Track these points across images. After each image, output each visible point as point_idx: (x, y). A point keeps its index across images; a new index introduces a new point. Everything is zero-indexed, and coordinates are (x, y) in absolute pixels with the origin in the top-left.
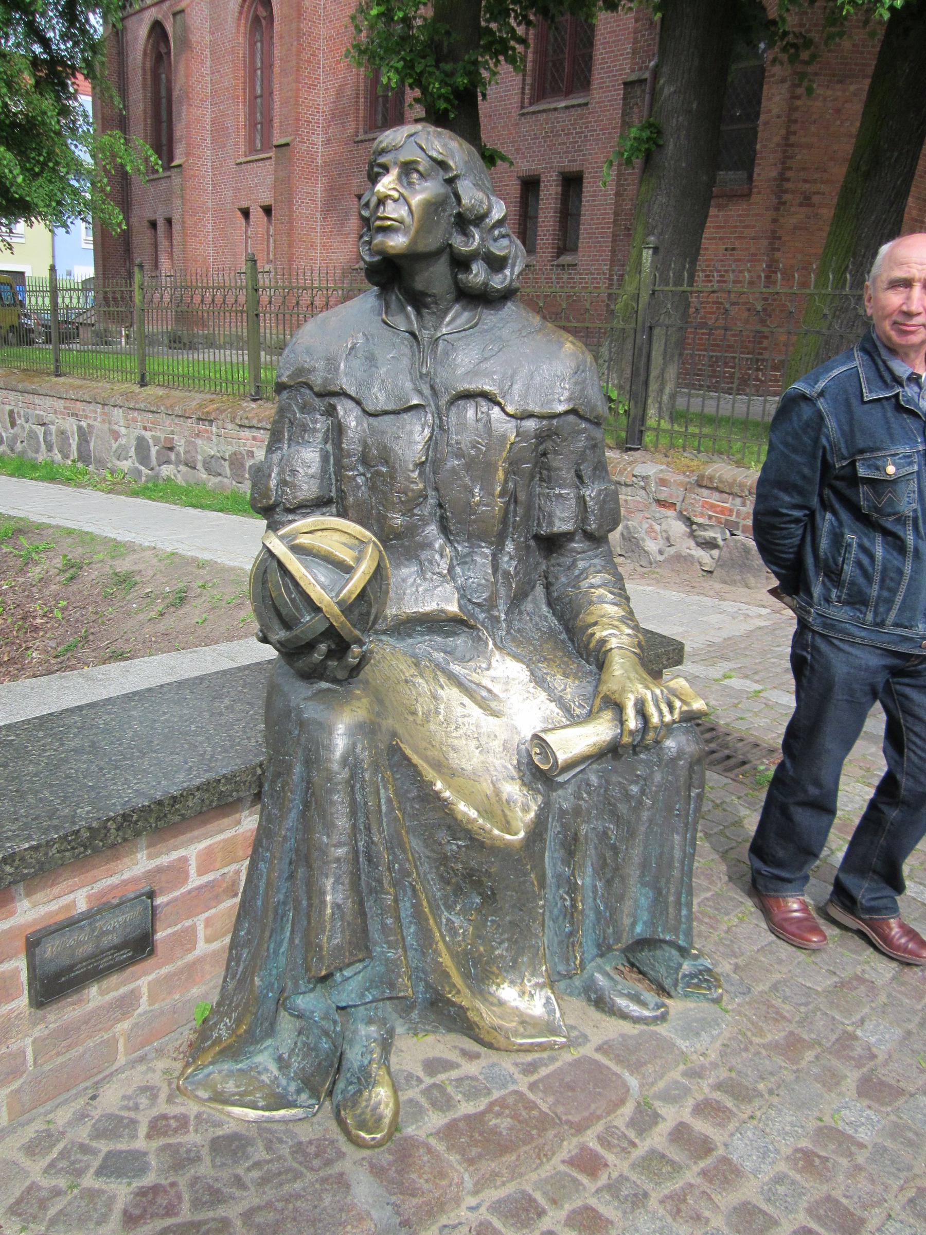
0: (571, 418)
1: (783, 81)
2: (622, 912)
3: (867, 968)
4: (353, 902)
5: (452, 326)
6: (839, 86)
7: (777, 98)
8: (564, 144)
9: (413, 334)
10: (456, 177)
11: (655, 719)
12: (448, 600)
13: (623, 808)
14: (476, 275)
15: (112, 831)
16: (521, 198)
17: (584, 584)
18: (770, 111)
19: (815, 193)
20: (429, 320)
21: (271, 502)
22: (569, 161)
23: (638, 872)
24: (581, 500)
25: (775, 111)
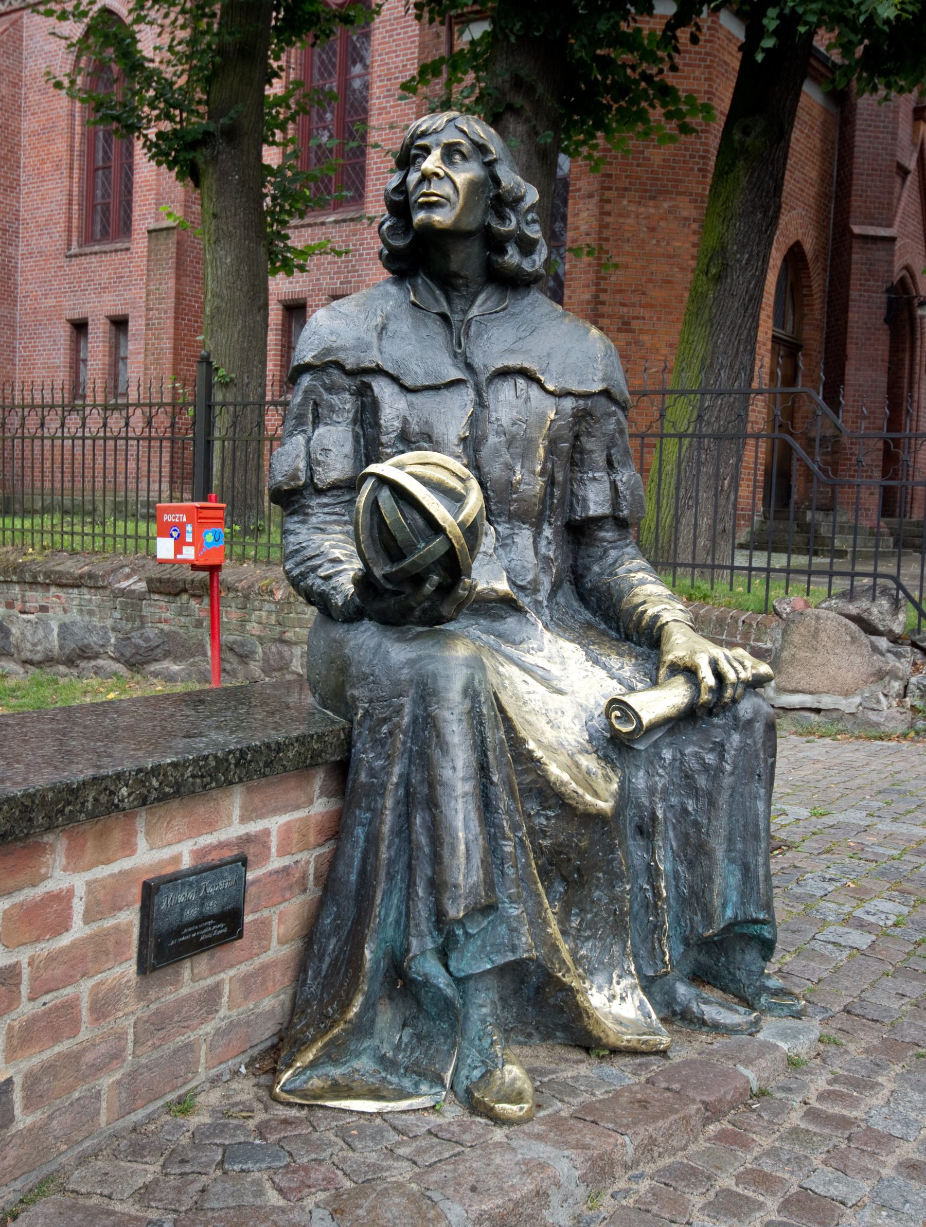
0: (603, 400)
1: (590, 196)
2: (712, 891)
3: (831, 1188)
4: (484, 839)
5: (485, 307)
6: (651, 203)
7: (584, 215)
8: (336, 263)
9: (444, 317)
10: (495, 160)
11: (731, 676)
12: (497, 579)
13: (702, 782)
14: (512, 256)
15: (232, 766)
16: (283, 325)
17: (621, 571)
18: (577, 228)
19: (634, 318)
20: (459, 304)
21: (301, 483)
22: (341, 283)
23: (724, 846)
24: (614, 486)
25: (584, 228)
